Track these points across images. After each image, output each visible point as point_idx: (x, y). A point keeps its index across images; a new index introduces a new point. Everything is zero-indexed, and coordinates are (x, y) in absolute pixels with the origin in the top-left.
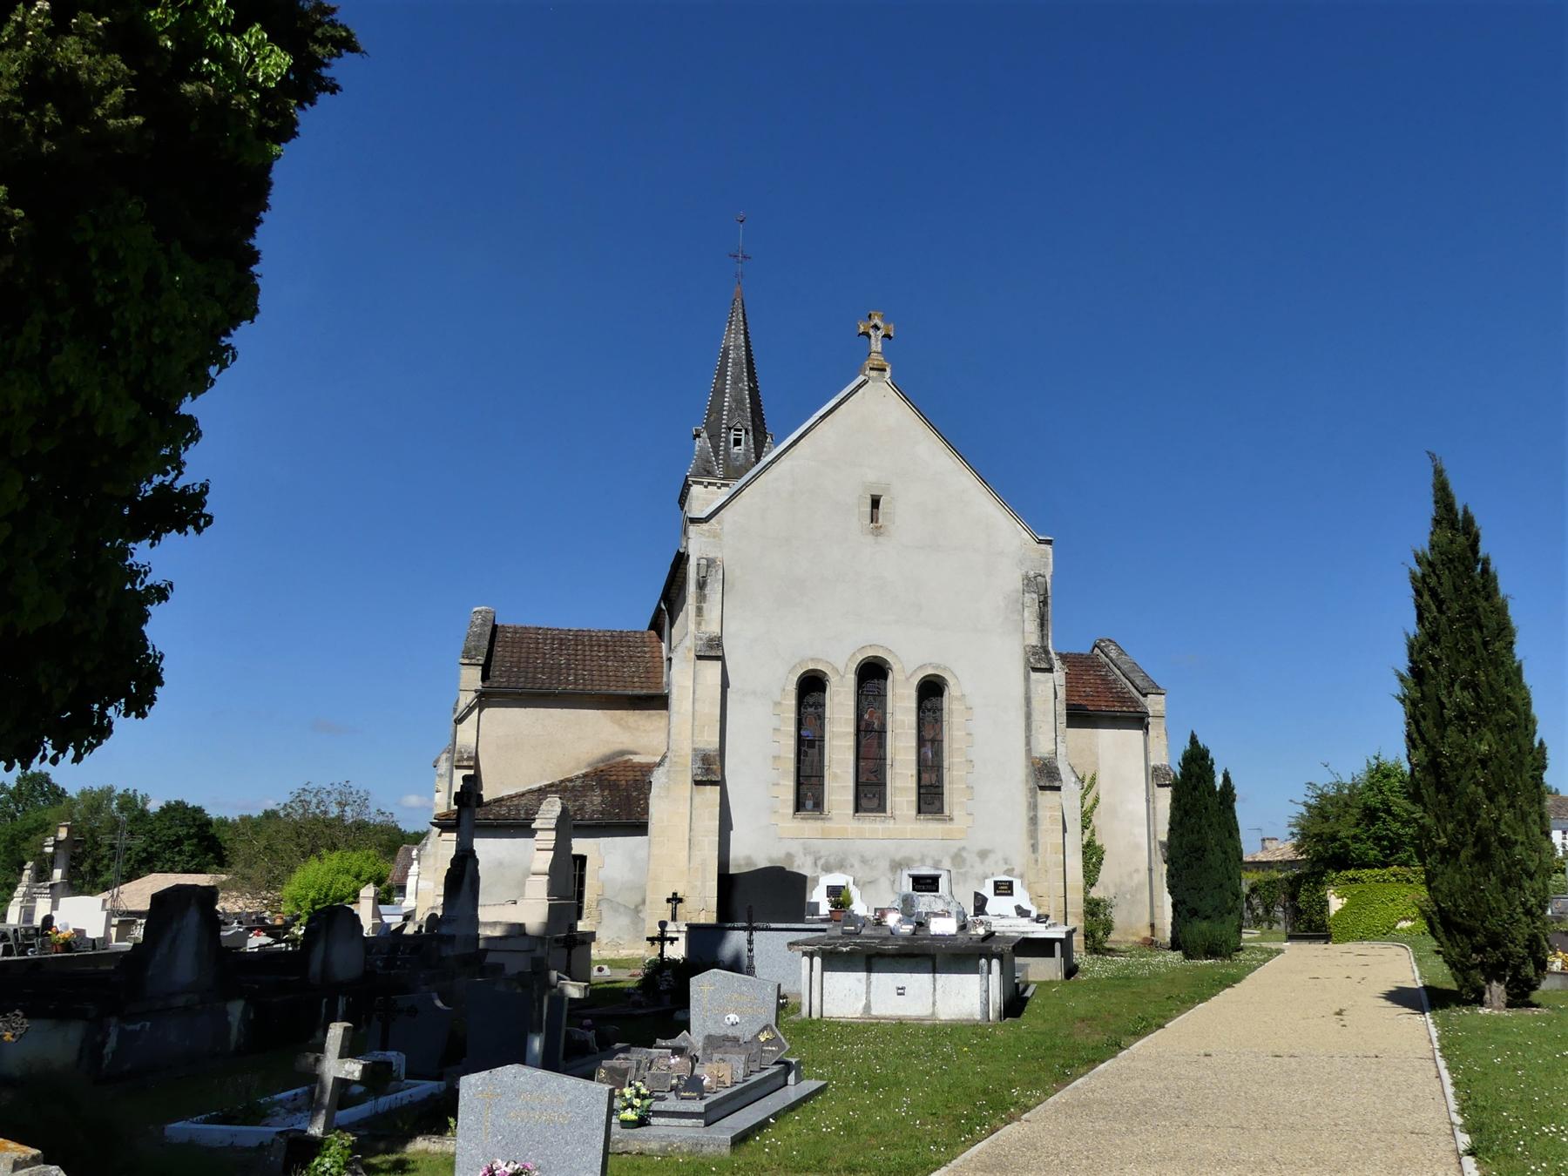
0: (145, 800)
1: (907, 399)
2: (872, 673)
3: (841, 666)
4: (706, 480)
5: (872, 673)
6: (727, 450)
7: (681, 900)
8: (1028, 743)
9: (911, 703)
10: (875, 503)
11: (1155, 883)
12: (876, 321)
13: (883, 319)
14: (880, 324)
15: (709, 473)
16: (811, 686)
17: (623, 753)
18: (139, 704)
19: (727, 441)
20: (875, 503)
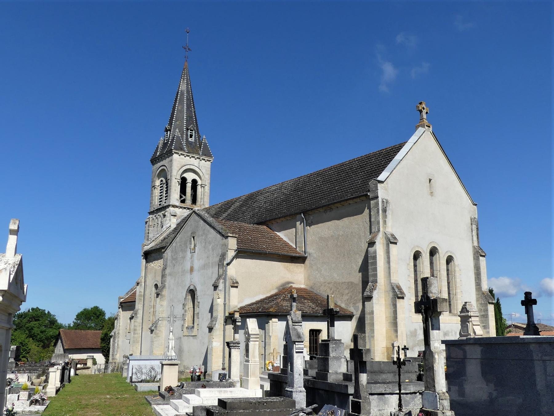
0: (45, 310)
1: (437, 140)
2: (433, 252)
3: (425, 249)
4: (180, 152)
5: (433, 252)
6: (187, 139)
7: (408, 349)
8: (415, 271)
9: (445, 262)
10: (430, 180)
11: (127, 304)
12: (424, 106)
13: (426, 106)
14: (425, 107)
15: (182, 149)
16: (417, 256)
17: (289, 283)
18: (522, 301)
19: (187, 135)
20: (430, 180)
